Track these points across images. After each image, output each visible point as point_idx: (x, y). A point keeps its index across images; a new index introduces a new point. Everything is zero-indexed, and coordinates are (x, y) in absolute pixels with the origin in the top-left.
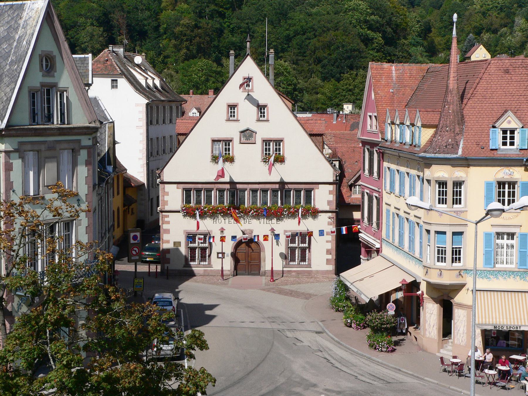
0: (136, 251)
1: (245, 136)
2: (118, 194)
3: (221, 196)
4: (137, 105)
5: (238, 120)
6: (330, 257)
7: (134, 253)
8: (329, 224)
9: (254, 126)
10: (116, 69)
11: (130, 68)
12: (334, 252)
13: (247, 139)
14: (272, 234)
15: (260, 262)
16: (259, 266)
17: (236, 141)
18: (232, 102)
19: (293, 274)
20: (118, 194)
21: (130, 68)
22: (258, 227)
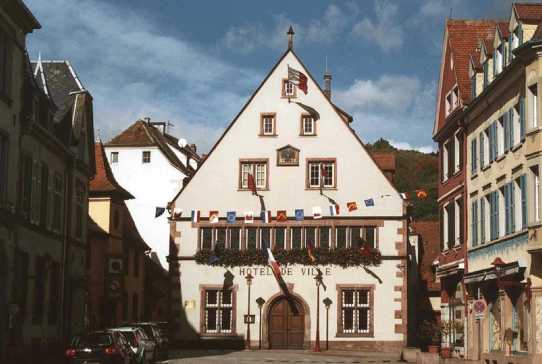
0: (116, 285)
1: (284, 156)
2: (136, 275)
3: (252, 238)
4: (173, 181)
5: (275, 135)
6: (399, 322)
7: (113, 287)
8: (399, 275)
9: (296, 142)
10: (149, 139)
11: (169, 145)
12: (405, 316)
13: (287, 160)
14: (317, 287)
15: (303, 329)
16: (302, 335)
17: (273, 162)
18: (268, 111)
19: (349, 346)
20: (136, 275)
21: (169, 145)
22: (300, 279)
